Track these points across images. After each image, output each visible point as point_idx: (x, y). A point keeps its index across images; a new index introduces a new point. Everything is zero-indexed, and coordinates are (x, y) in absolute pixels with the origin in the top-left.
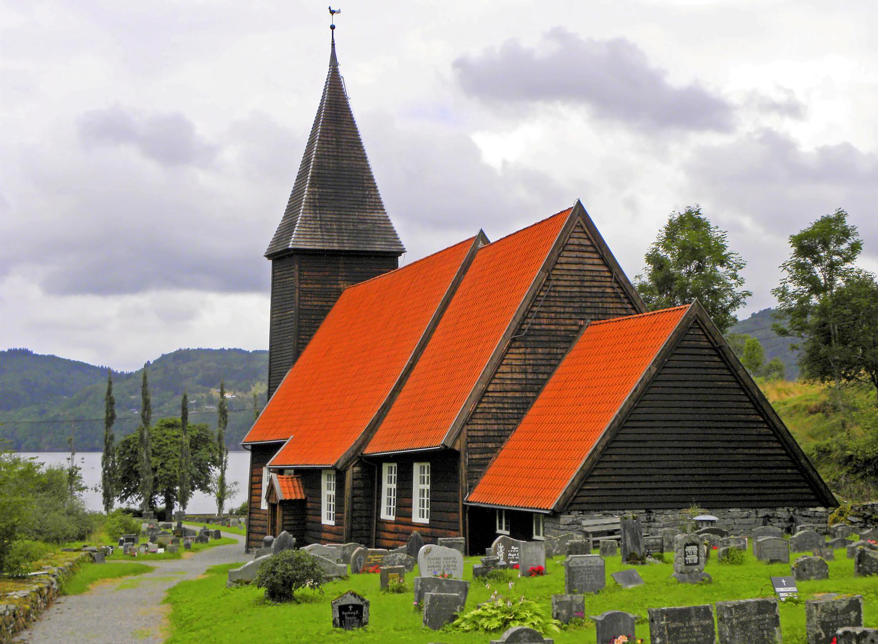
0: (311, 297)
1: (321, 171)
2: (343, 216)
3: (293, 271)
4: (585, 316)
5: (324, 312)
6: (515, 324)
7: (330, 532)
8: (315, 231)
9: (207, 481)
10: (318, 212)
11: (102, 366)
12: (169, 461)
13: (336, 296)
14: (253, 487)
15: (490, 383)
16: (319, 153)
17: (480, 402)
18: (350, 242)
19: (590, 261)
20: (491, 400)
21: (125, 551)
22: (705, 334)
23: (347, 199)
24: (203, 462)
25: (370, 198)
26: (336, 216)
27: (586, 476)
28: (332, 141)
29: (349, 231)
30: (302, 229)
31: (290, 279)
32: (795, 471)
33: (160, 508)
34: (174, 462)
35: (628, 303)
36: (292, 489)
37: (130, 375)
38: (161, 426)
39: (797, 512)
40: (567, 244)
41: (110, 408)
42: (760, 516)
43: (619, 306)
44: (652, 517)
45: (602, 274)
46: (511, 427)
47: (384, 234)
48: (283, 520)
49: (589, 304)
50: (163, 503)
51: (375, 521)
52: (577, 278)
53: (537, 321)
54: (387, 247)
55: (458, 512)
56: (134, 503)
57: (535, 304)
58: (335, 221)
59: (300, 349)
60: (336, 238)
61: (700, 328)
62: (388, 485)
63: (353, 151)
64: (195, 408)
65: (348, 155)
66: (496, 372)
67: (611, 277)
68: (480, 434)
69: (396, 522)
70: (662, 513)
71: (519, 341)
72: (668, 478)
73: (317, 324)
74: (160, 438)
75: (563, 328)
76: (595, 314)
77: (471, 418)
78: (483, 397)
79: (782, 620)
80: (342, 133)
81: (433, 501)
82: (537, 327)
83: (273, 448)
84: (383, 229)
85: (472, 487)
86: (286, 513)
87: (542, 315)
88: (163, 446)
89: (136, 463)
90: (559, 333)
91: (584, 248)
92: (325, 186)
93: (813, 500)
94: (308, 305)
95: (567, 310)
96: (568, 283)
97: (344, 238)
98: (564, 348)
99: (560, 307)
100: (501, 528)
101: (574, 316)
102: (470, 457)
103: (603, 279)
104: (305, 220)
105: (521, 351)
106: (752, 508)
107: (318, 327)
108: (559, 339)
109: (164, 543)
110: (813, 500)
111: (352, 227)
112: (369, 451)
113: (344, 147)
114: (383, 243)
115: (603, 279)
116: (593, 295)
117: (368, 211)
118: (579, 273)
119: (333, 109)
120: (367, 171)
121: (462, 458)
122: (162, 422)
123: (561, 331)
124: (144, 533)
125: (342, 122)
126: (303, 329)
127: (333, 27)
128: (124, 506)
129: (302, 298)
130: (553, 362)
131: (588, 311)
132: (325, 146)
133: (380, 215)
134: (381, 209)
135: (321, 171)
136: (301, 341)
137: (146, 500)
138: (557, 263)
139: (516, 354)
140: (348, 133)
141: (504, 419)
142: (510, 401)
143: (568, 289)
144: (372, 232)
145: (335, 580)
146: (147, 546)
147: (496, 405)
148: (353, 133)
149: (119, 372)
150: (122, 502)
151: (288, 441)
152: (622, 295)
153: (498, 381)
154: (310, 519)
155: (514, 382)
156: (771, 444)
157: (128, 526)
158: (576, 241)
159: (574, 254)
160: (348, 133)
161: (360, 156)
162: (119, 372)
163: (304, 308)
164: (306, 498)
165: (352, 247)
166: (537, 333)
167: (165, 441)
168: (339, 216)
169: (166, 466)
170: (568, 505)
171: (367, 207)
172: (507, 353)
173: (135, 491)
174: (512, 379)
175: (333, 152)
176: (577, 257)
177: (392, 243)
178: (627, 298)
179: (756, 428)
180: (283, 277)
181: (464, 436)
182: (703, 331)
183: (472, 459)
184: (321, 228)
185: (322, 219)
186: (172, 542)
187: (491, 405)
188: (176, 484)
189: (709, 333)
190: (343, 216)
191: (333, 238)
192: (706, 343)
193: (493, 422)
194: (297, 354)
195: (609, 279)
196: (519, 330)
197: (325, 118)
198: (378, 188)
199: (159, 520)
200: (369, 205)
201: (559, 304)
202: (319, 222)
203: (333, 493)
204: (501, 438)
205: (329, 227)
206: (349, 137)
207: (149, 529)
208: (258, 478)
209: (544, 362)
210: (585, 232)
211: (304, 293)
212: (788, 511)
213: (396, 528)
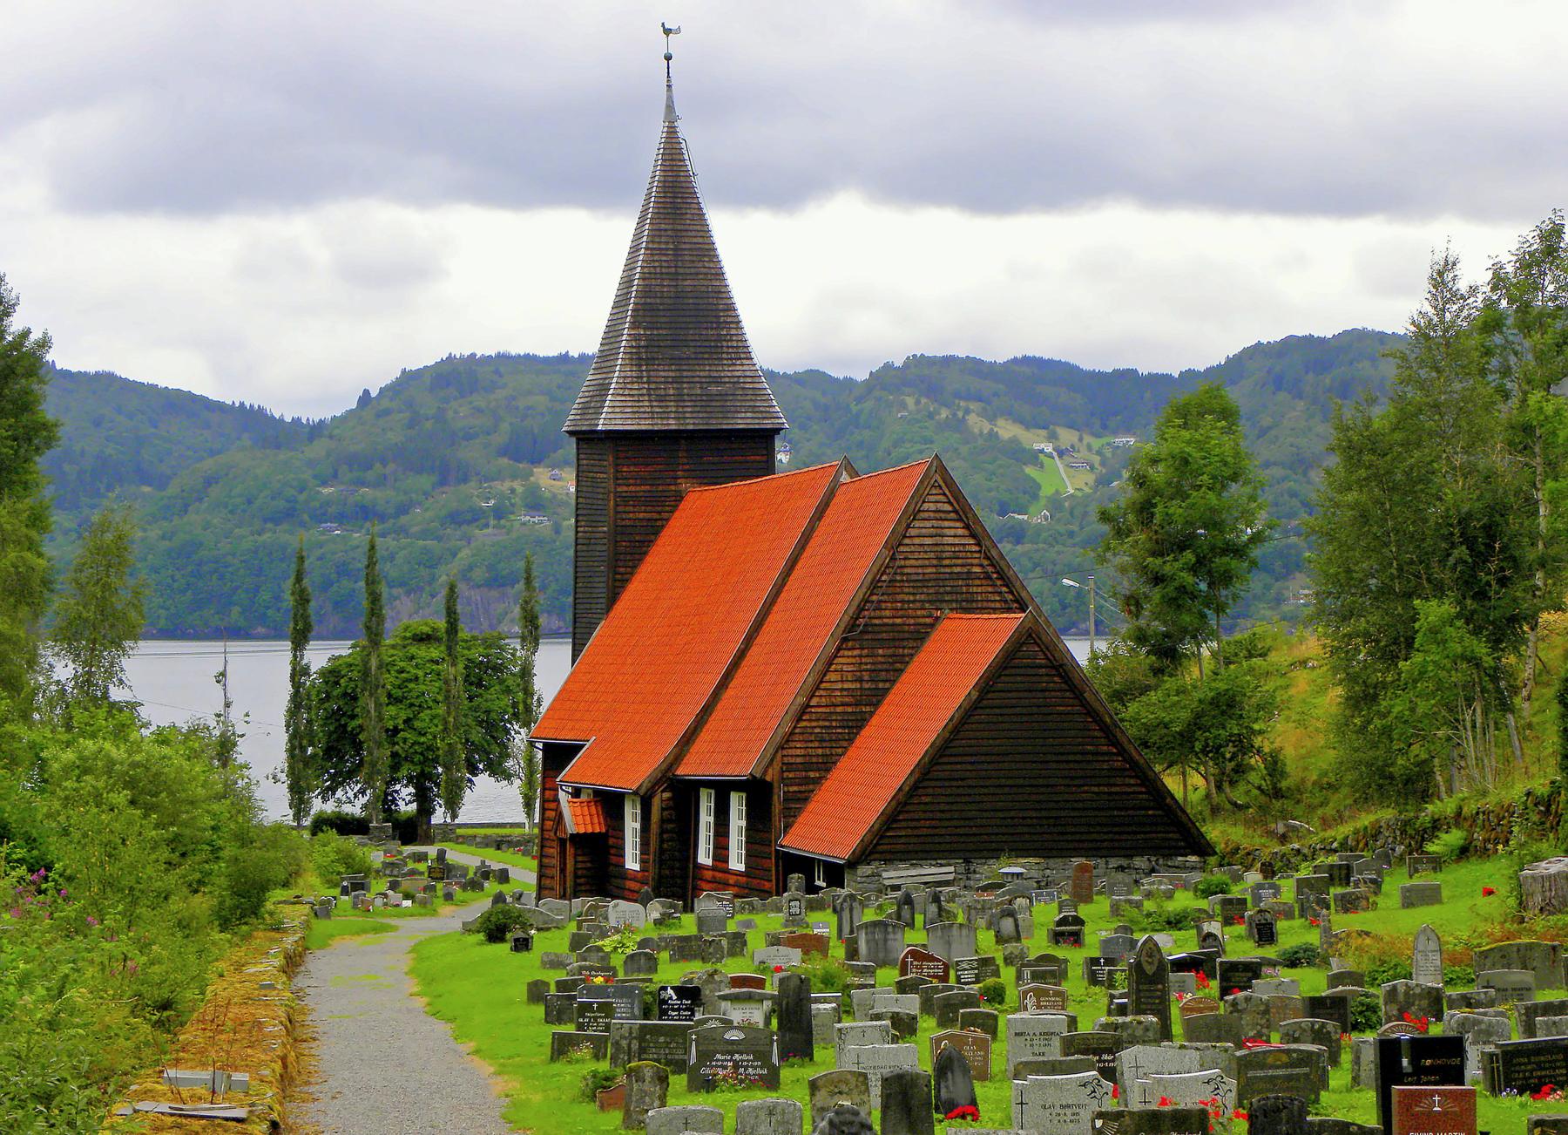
0: (634, 506)
1: (648, 300)
2: (685, 374)
3: (605, 463)
4: (944, 605)
5: (653, 530)
6: (847, 618)
7: (634, 879)
8: (639, 401)
9: (505, 755)
10: (644, 368)
11: (242, 404)
12: (422, 714)
13: (672, 503)
14: (546, 806)
15: (813, 696)
16: (646, 270)
17: (799, 720)
18: (694, 415)
19: (952, 532)
20: (814, 717)
21: (355, 906)
22: (1042, 651)
23: (692, 344)
24: (493, 715)
25: (728, 341)
26: (673, 374)
27: (890, 819)
28: (667, 249)
29: (694, 398)
30: (619, 398)
31: (602, 476)
32: (1160, 812)
33: (406, 812)
34: (434, 717)
35: (1004, 586)
36: (588, 818)
37: (317, 430)
38: (405, 638)
39: (1161, 861)
40: (919, 511)
41: (301, 611)
42: (1111, 866)
43: (990, 589)
44: (972, 868)
45: (967, 548)
46: (840, 751)
47: (751, 400)
48: (576, 862)
49: (948, 589)
50: (410, 802)
51: (691, 866)
52: (932, 555)
53: (878, 613)
54: (757, 421)
55: (770, 859)
56: (350, 802)
57: (875, 591)
58: (671, 383)
59: (617, 590)
60: (674, 410)
61: (1035, 643)
63: (700, 264)
64: (492, 522)
65: (693, 271)
66: (822, 682)
67: (980, 552)
68: (799, 760)
69: (713, 868)
70: (985, 864)
71: (854, 640)
72: (993, 822)
73: (645, 549)
74: (402, 664)
75: (912, 621)
76: (957, 601)
77: (788, 741)
78: (804, 713)
79: (748, 943)
80: (684, 234)
81: (752, 843)
84: (750, 392)
85: (788, 826)
86: (579, 852)
87: (883, 606)
88: (410, 681)
89: (353, 717)
90: (906, 628)
91: (943, 516)
92: (655, 325)
93: (1184, 848)
94: (630, 519)
95: (918, 597)
96: (920, 563)
97: (686, 409)
98: (913, 648)
99: (910, 594)
100: (819, 879)
101: (927, 605)
102: (786, 789)
103: (969, 555)
104: (624, 383)
105: (856, 652)
106: (1101, 857)
107: (645, 553)
108: (907, 635)
109: (412, 891)
110: (1184, 848)
111: (699, 392)
112: (682, 771)
113: (687, 258)
114: (749, 415)
115: (969, 555)
116: (955, 576)
117: (725, 362)
118: (936, 549)
119: (669, 195)
120: (724, 295)
121: (776, 790)
122: (406, 630)
123: (909, 625)
124: (378, 872)
125: (684, 217)
126: (622, 557)
127: (668, 58)
128: (329, 807)
129: (620, 509)
130: (898, 666)
131: (947, 598)
132: (656, 258)
133: (745, 368)
134: (747, 359)
135: (648, 300)
136: (618, 577)
137: (376, 797)
138: (905, 537)
139: (848, 657)
140: (693, 234)
142: (839, 718)
143: (920, 571)
144: (731, 398)
145: (553, 930)
146: (385, 896)
147: (821, 723)
148: (702, 234)
149: (288, 419)
150: (325, 800)
151: (588, 744)
153: (822, 693)
155: (845, 693)
156: (1128, 781)
157: (350, 860)
158: (932, 507)
159: (928, 524)
160: (693, 234)
161: (713, 271)
162: (288, 419)
163: (624, 523)
164: (607, 831)
165: (699, 424)
166: (876, 629)
167: (414, 671)
168: (678, 374)
169: (417, 724)
170: (865, 854)
171: (724, 356)
172: (836, 657)
173: (350, 775)
174: (842, 690)
175: (669, 267)
176: (933, 527)
177: (764, 415)
178: (1002, 578)
179: (1108, 761)
180: (591, 469)
181: (777, 766)
182: (1039, 646)
183: (789, 792)
184: (649, 395)
186: (425, 889)
187: (814, 724)
188: (436, 761)
189: (1047, 649)
190: (685, 374)
191: (669, 410)
192: (1043, 661)
193: (817, 744)
194: (613, 598)
195: (977, 555)
196: (852, 626)
197: (656, 211)
198: (744, 324)
199: (404, 843)
200: (727, 353)
201: (906, 590)
203: (638, 825)
204: (826, 765)
205: (662, 392)
206: (695, 240)
207: (386, 865)
208: (552, 792)
209: (885, 666)
210: (945, 494)
211: (623, 500)
212: (1149, 860)
213: (714, 877)
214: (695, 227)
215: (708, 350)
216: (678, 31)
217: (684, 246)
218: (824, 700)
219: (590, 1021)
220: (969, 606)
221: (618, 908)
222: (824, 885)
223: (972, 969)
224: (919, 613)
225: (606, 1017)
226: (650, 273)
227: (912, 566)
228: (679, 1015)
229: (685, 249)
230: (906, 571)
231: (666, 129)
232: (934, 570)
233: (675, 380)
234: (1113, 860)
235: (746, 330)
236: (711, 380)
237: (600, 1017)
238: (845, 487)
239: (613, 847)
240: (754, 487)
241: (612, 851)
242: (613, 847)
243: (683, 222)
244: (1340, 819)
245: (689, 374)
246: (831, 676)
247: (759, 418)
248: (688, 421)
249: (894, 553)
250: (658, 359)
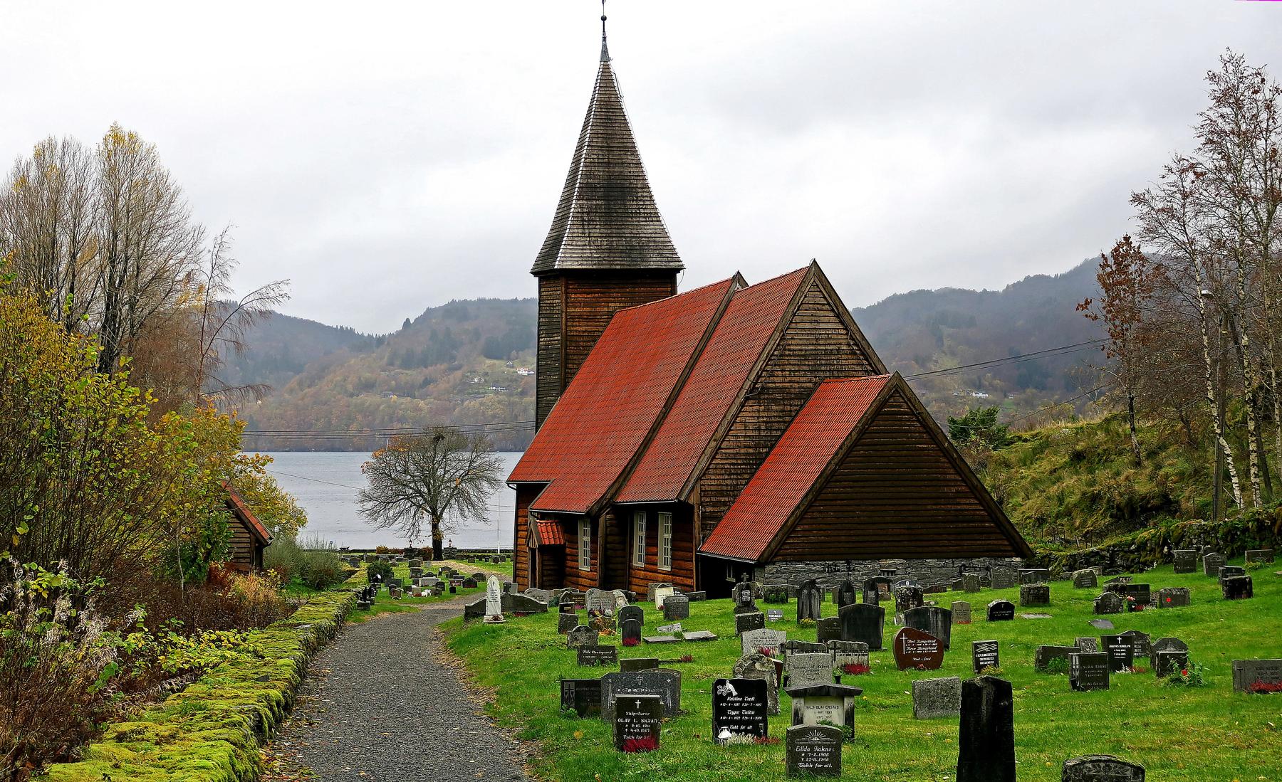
11: (341, 327)
16: (588, 160)
17: (714, 458)
19: (826, 319)
22: (905, 402)
27: (788, 530)
37: (380, 341)
43: (854, 362)
44: (852, 567)
49: (824, 362)
55: (692, 561)
58: (606, 237)
62: (640, 534)
65: (620, 161)
67: (847, 334)
69: (645, 570)
71: (753, 399)
76: (830, 371)
77: (704, 474)
82: (770, 385)
83: (539, 487)
91: (819, 307)
100: (730, 576)
112: (620, 500)
121: (696, 510)
127: (604, 19)
133: (657, 227)
141: (737, 474)
149: (366, 335)
152: (858, 352)
154: (569, 565)
162: (366, 335)
164: (565, 544)
174: (745, 436)
181: (698, 490)
185: (592, 235)
187: (724, 462)
194: (564, 385)
195: (845, 337)
196: (752, 389)
202: (588, 239)
204: (735, 492)
210: (821, 291)
218: (731, 443)
219: (632, 722)
220: (840, 375)
221: (593, 595)
222: (734, 580)
223: (992, 651)
224: (801, 379)
225: (651, 717)
227: (796, 344)
228: (740, 715)
230: (792, 348)
232: (813, 348)
234: (956, 561)
237: (645, 717)
238: (739, 294)
239: (569, 555)
240: (666, 304)
241: (569, 558)
242: (569, 555)
244: (1101, 535)
246: (738, 426)
249: (783, 335)
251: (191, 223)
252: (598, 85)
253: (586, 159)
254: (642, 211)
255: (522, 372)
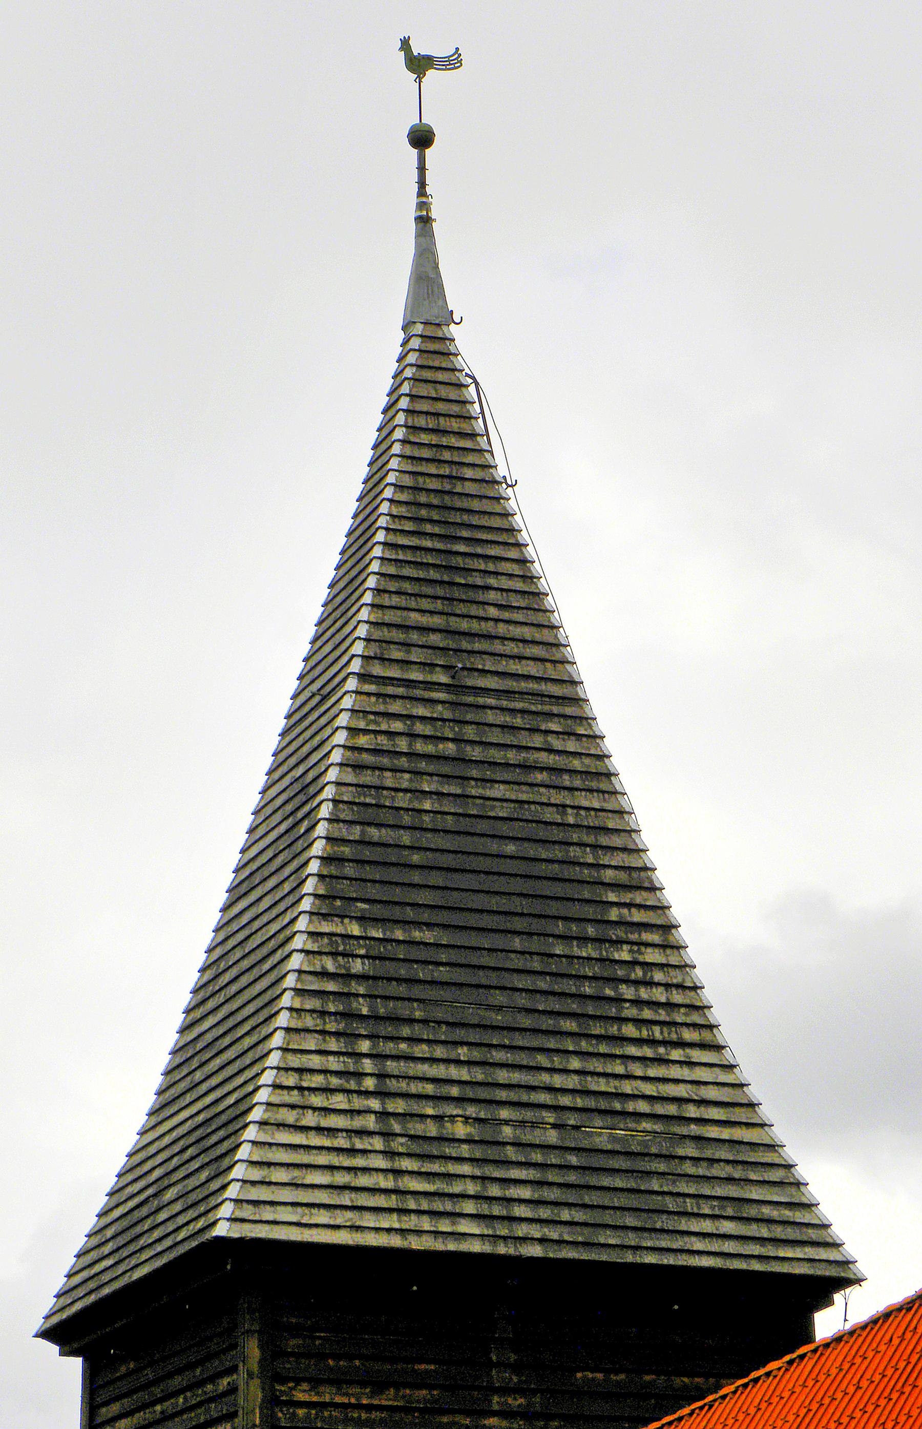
1: (374, 833)
2: (503, 1076)
8: (352, 1152)
16: (363, 741)
18: (544, 1213)
26: (463, 1074)
47: (730, 1180)
54: (756, 1249)
58: (460, 1100)
63: (537, 741)
65: (512, 756)
113: (491, 717)
114: (728, 1227)
117: (633, 1050)
120: (617, 841)
125: (481, 596)
132: (396, 707)
134: (703, 1046)
135: (374, 833)
140: (511, 648)
171: (630, 1030)
177: (779, 1232)
184: (387, 1135)
190: (503, 1076)
191: (457, 1188)
198: (684, 934)
200: (639, 1022)
205: (432, 1129)
206: (514, 667)
214: (517, 631)
215: (574, 1007)
216: (453, 62)
217: (482, 682)
226: (375, 751)
229: (486, 691)
231: (415, 343)
233: (470, 1093)
235: (693, 954)
236: (591, 1103)
243: (474, 610)
245: (516, 1077)
247: (762, 1240)
248: (522, 1230)
250: (411, 1021)
251: (454, 1183)
252: (401, 418)
253: (353, 731)
254: (628, 992)
255: (391, 1005)
